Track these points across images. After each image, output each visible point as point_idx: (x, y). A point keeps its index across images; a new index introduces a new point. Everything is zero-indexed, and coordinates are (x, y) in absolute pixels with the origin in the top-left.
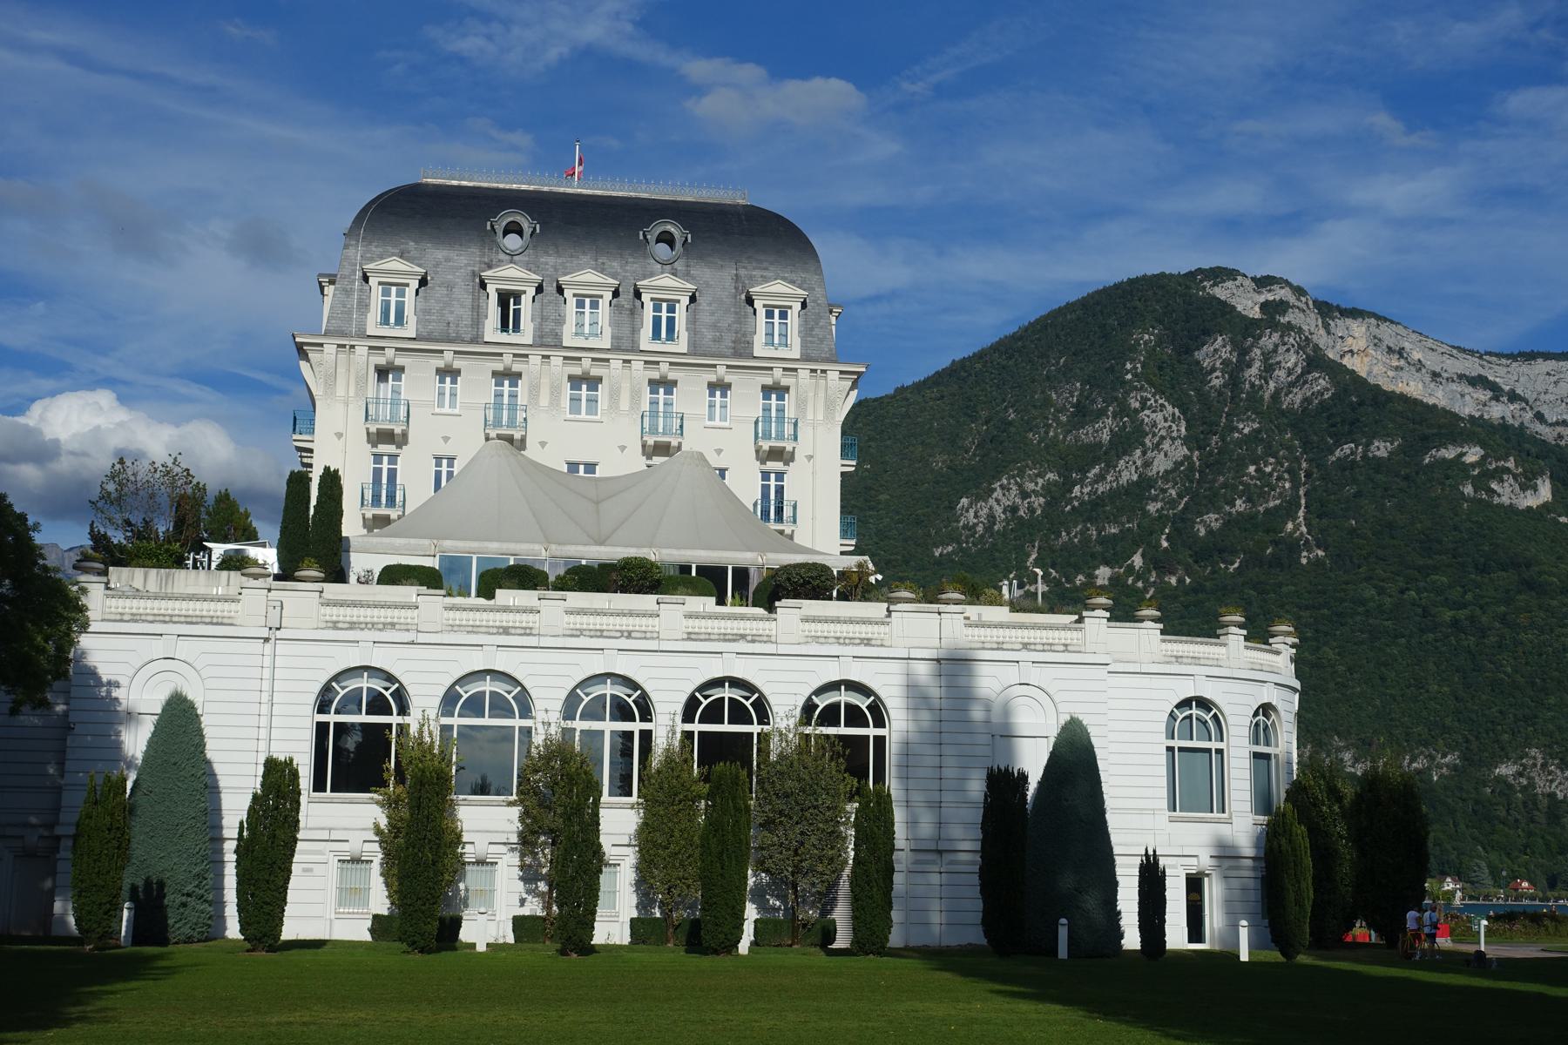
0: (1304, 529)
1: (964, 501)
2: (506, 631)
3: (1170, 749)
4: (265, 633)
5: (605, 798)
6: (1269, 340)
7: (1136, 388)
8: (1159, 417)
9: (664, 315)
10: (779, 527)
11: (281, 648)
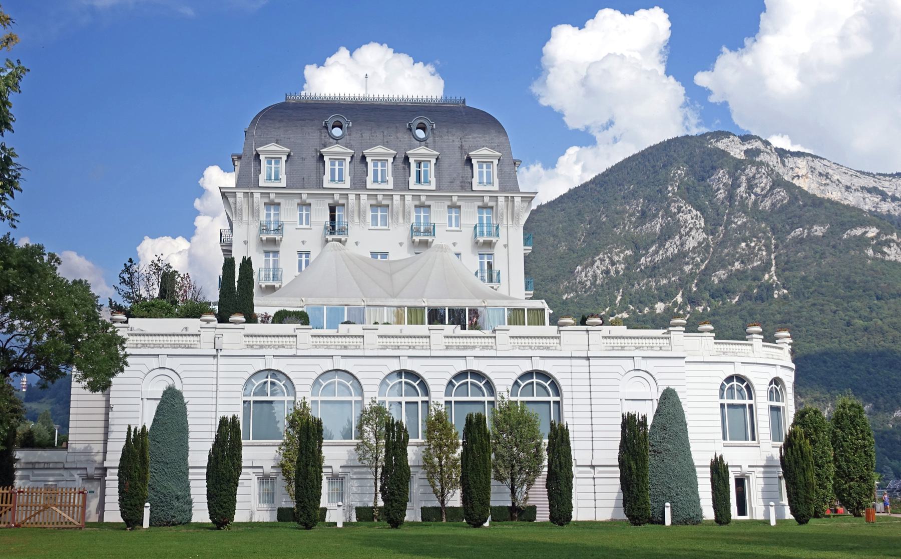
0: (775, 278)
1: (579, 268)
2: (346, 347)
3: (722, 406)
4: (214, 352)
6: (751, 171)
7: (674, 201)
8: (688, 217)
10: (492, 285)
11: (221, 361)
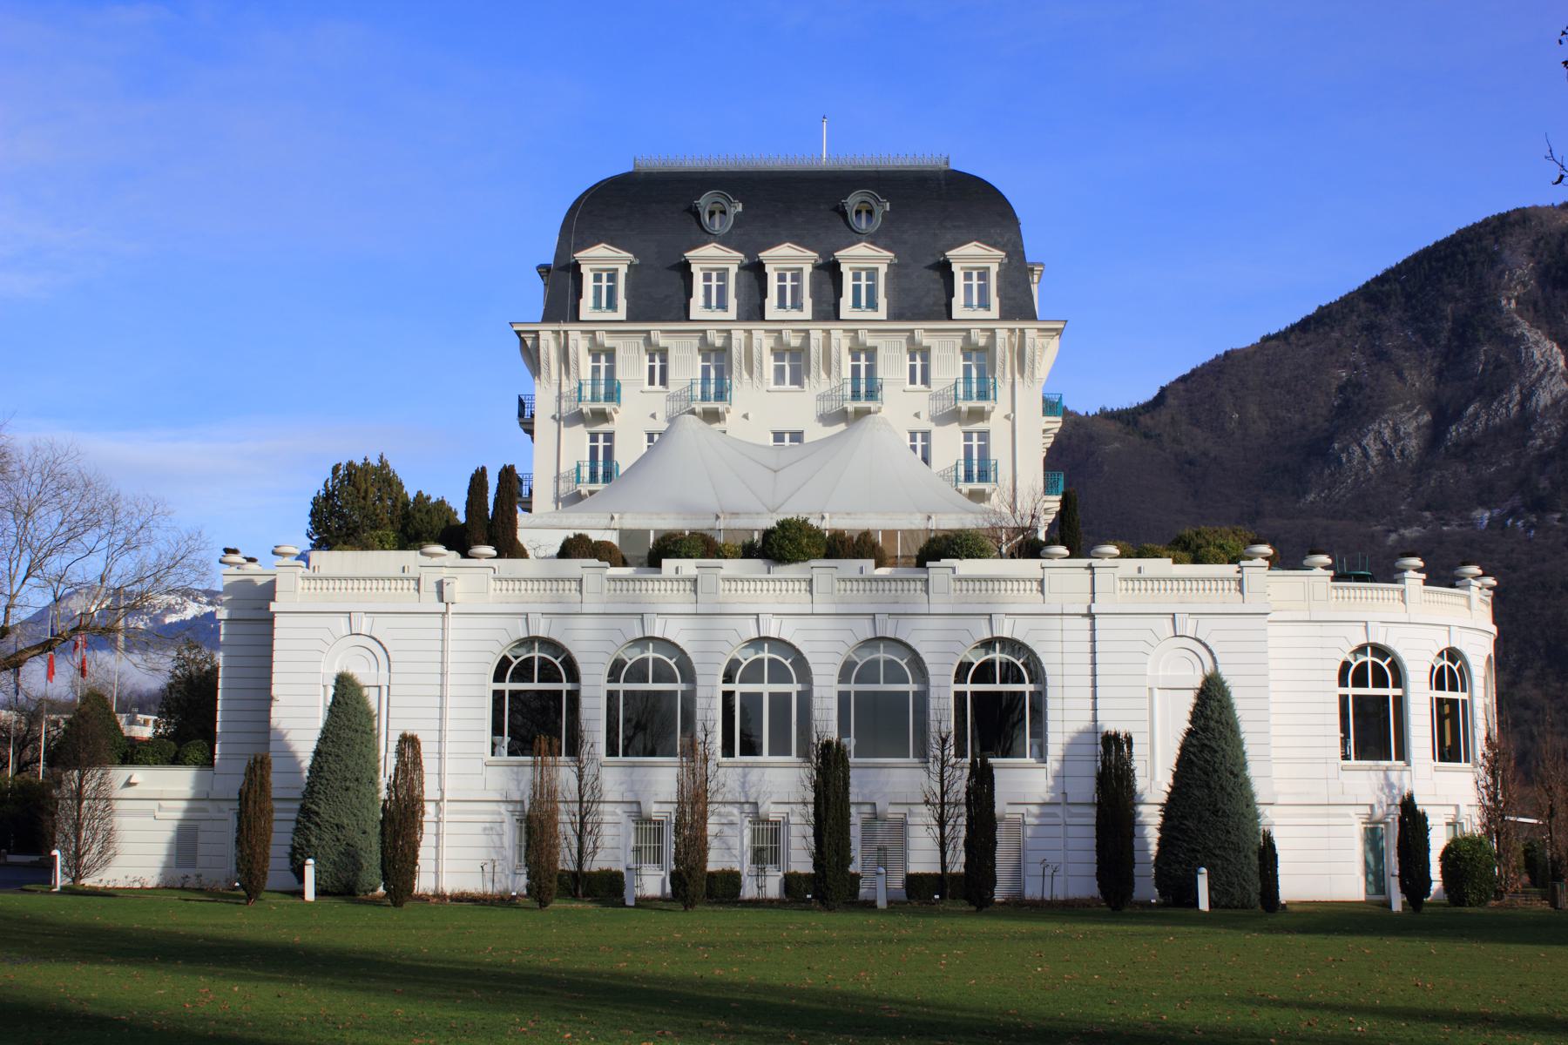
4: (442, 607)
5: (852, 760)
9: (789, 283)
